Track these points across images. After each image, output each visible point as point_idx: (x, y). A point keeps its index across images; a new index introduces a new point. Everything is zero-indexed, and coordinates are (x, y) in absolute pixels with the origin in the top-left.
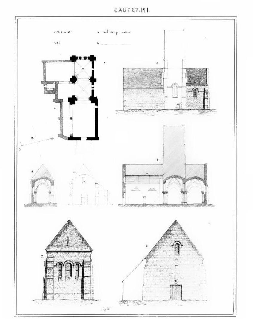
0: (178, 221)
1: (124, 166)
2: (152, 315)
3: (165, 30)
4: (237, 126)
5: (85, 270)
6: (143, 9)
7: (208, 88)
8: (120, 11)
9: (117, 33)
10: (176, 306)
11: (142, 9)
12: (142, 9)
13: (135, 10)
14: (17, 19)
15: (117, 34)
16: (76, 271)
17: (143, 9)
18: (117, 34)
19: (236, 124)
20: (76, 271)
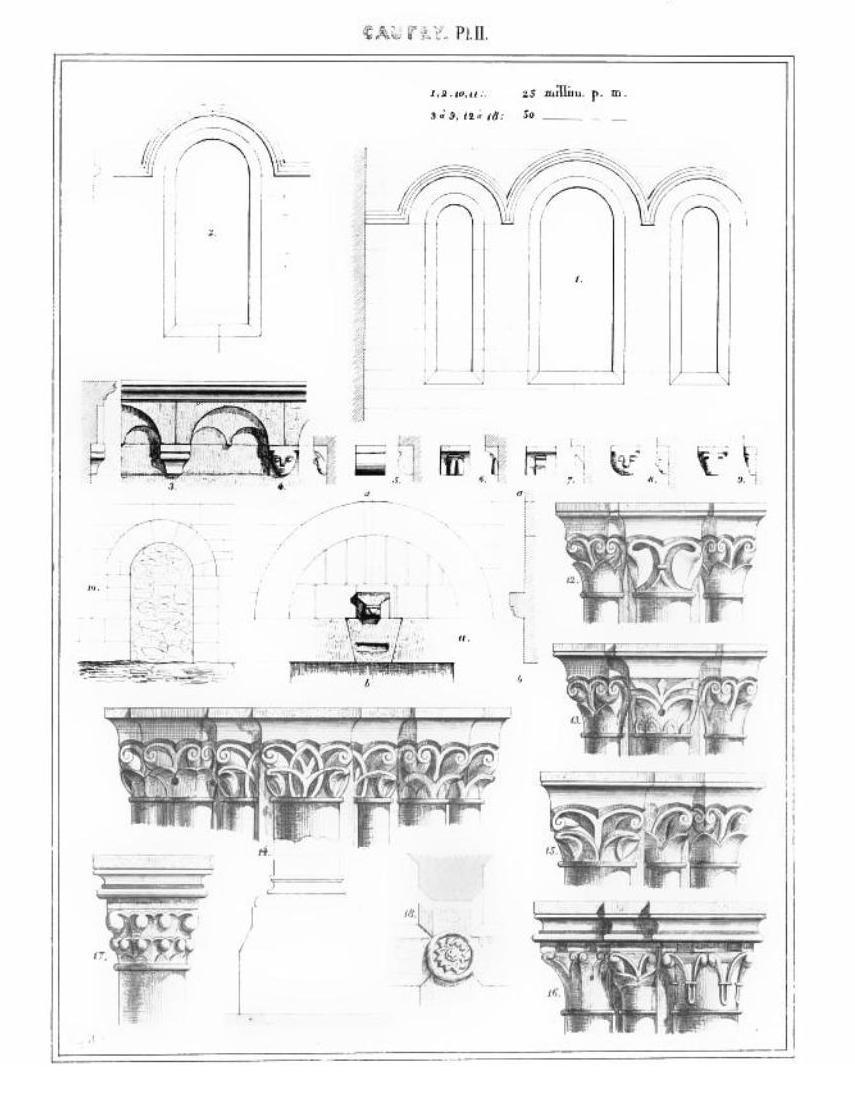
0: (746, 840)
1: (741, 600)
2: (575, 932)
3: (308, 176)
4: (795, 695)
5: (368, 716)
6: (460, 31)
7: (189, 453)
8: (382, 38)
9: (595, 93)
10: (416, 914)
11: (460, 30)
12: (460, 30)
13: (432, 33)
14: (58, 62)
15: (593, 100)
16: (412, 710)
17: (460, 31)
18: (593, 100)
19: (793, 691)
20: (412, 710)
